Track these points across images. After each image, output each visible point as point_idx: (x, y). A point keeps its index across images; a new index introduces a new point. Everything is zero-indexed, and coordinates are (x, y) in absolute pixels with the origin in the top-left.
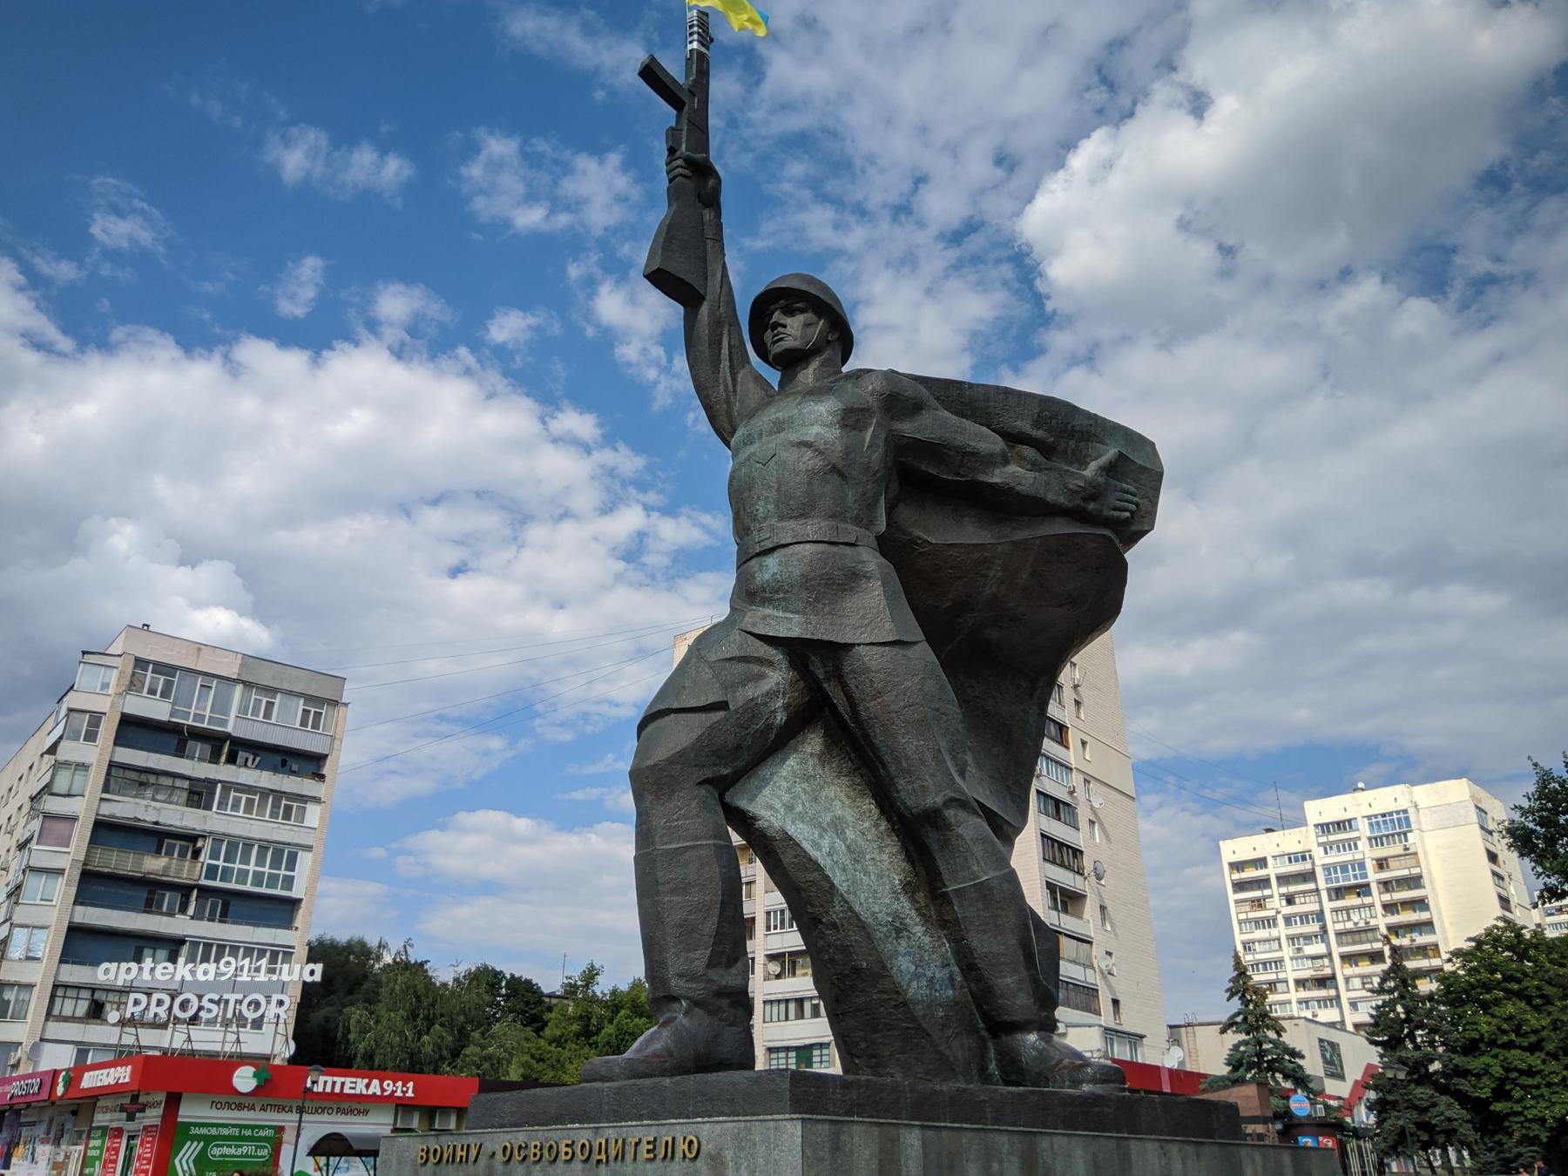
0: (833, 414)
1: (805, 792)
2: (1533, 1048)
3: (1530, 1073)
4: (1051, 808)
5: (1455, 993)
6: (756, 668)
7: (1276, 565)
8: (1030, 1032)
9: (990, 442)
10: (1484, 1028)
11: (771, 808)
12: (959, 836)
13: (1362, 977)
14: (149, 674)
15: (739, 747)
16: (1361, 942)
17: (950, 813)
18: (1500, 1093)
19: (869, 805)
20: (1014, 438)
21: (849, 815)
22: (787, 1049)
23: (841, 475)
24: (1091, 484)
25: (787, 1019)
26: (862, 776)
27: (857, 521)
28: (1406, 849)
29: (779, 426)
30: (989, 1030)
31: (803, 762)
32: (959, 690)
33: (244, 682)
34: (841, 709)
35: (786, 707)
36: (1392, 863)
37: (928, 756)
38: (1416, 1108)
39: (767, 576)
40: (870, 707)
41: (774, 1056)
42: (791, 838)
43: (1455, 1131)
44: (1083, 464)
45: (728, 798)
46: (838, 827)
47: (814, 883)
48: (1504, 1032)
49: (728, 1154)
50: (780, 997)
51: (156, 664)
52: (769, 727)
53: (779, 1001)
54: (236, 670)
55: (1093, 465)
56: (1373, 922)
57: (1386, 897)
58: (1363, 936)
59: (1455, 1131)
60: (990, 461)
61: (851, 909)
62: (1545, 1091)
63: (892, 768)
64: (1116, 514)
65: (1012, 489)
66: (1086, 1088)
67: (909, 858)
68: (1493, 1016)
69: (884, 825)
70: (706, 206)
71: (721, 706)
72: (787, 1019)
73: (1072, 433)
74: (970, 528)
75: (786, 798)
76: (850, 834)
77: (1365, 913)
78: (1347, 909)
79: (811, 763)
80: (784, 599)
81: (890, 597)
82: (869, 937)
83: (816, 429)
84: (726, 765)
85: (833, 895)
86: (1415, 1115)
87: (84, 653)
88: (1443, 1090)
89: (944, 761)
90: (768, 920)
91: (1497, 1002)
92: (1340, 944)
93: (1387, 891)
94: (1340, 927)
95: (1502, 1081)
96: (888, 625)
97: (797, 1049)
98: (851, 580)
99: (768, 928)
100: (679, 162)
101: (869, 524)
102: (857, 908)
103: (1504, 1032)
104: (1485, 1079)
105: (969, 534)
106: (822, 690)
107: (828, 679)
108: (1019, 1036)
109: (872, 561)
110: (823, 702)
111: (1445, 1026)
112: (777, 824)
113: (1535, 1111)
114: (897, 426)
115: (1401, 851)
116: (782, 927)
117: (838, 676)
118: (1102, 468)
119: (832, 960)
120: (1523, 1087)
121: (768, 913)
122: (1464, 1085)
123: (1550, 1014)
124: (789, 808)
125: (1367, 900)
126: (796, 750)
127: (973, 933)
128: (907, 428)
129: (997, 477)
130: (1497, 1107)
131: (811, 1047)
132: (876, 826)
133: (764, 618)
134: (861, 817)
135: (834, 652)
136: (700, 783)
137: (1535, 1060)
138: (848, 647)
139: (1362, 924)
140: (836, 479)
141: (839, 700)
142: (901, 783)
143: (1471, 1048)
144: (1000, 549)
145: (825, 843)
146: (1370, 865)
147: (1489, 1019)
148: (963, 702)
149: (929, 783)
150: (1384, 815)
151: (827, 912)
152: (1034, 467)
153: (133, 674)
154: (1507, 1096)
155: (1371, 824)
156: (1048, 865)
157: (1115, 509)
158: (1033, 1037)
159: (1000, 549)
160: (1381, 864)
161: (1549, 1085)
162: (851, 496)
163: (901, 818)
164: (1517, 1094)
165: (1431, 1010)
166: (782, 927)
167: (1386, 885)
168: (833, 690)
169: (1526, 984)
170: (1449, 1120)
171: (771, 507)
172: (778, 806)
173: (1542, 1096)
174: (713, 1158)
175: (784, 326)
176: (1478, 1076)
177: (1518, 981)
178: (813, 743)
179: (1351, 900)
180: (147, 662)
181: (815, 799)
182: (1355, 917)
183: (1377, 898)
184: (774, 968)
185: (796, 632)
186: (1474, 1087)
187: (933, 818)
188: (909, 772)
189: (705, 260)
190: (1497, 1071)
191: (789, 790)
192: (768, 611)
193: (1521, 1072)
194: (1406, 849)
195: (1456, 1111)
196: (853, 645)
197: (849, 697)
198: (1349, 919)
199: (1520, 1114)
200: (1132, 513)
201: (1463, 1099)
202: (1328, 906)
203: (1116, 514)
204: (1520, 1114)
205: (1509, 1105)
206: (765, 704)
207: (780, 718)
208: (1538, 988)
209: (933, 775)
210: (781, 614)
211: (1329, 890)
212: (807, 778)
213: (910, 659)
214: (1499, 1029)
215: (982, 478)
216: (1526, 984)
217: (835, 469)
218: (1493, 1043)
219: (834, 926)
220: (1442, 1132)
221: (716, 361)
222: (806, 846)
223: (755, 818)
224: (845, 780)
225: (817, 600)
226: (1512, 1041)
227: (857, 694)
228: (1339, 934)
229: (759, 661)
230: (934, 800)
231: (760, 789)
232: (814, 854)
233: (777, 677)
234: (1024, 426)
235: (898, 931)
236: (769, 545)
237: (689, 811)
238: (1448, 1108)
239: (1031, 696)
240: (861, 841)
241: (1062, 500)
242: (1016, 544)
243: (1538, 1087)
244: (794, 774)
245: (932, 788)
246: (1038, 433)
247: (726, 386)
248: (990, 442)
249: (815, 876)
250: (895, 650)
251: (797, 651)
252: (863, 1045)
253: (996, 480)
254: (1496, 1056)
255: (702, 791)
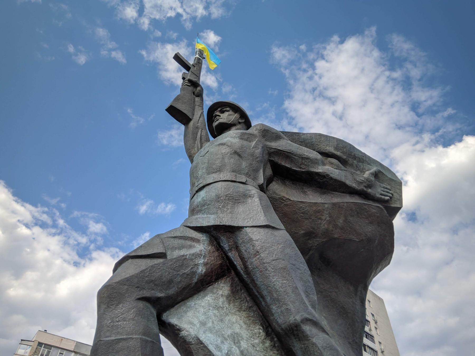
1: (215, 315)
6: (189, 243)
7: (453, 322)
8: (160, 32)
9: (314, 155)
11: (191, 323)
12: (314, 344)
14: (42, 348)
15: (170, 282)
17: (307, 328)
19: (258, 330)
21: (245, 333)
23: (239, 155)
24: (367, 180)
26: (254, 311)
27: (247, 175)
31: (216, 299)
32: (316, 284)
33: (75, 352)
34: (239, 268)
35: (205, 264)
37: (290, 291)
40: (253, 262)
42: (201, 343)
44: (363, 171)
45: (165, 317)
46: (236, 339)
51: (46, 344)
52: (194, 273)
54: (73, 347)
55: (367, 173)
63: (268, 299)
64: (383, 197)
65: (328, 175)
69: (268, 343)
70: (198, 96)
73: (355, 157)
74: (311, 197)
75: (202, 318)
76: (244, 344)
79: (221, 300)
84: (161, 291)
87: (22, 340)
89: (299, 294)
100: (187, 81)
101: (255, 179)
105: (312, 198)
106: (228, 258)
107: (230, 250)
110: (229, 267)
114: (268, 144)
118: (372, 174)
124: (203, 324)
126: (212, 292)
128: (274, 145)
129: (320, 169)
134: (253, 336)
135: (232, 230)
136: (140, 299)
138: (240, 228)
140: (237, 157)
141: (238, 263)
142: (274, 308)
144: (326, 206)
148: (319, 292)
149: (291, 306)
153: (37, 348)
157: (382, 195)
159: (326, 206)
162: (244, 164)
163: (278, 335)
168: (233, 255)
172: (196, 322)
175: (220, 116)
178: (222, 289)
180: (42, 344)
181: (222, 320)
187: (295, 331)
188: (278, 300)
189: (194, 110)
191: (205, 313)
196: (242, 227)
197: (242, 258)
200: (391, 198)
203: (383, 197)
206: (192, 260)
207: (201, 270)
209: (293, 302)
210: (205, 216)
212: (217, 308)
213: (275, 236)
217: (236, 153)
221: (195, 139)
222: (212, 348)
223: (180, 330)
224: (244, 314)
229: (192, 239)
231: (186, 312)
233: (201, 247)
236: (202, 185)
237: (131, 318)
239: (356, 295)
240: (251, 350)
241: (354, 185)
242: (334, 204)
244: (209, 305)
245: (293, 310)
246: (338, 153)
248: (314, 155)
250: (267, 230)
255: (141, 304)
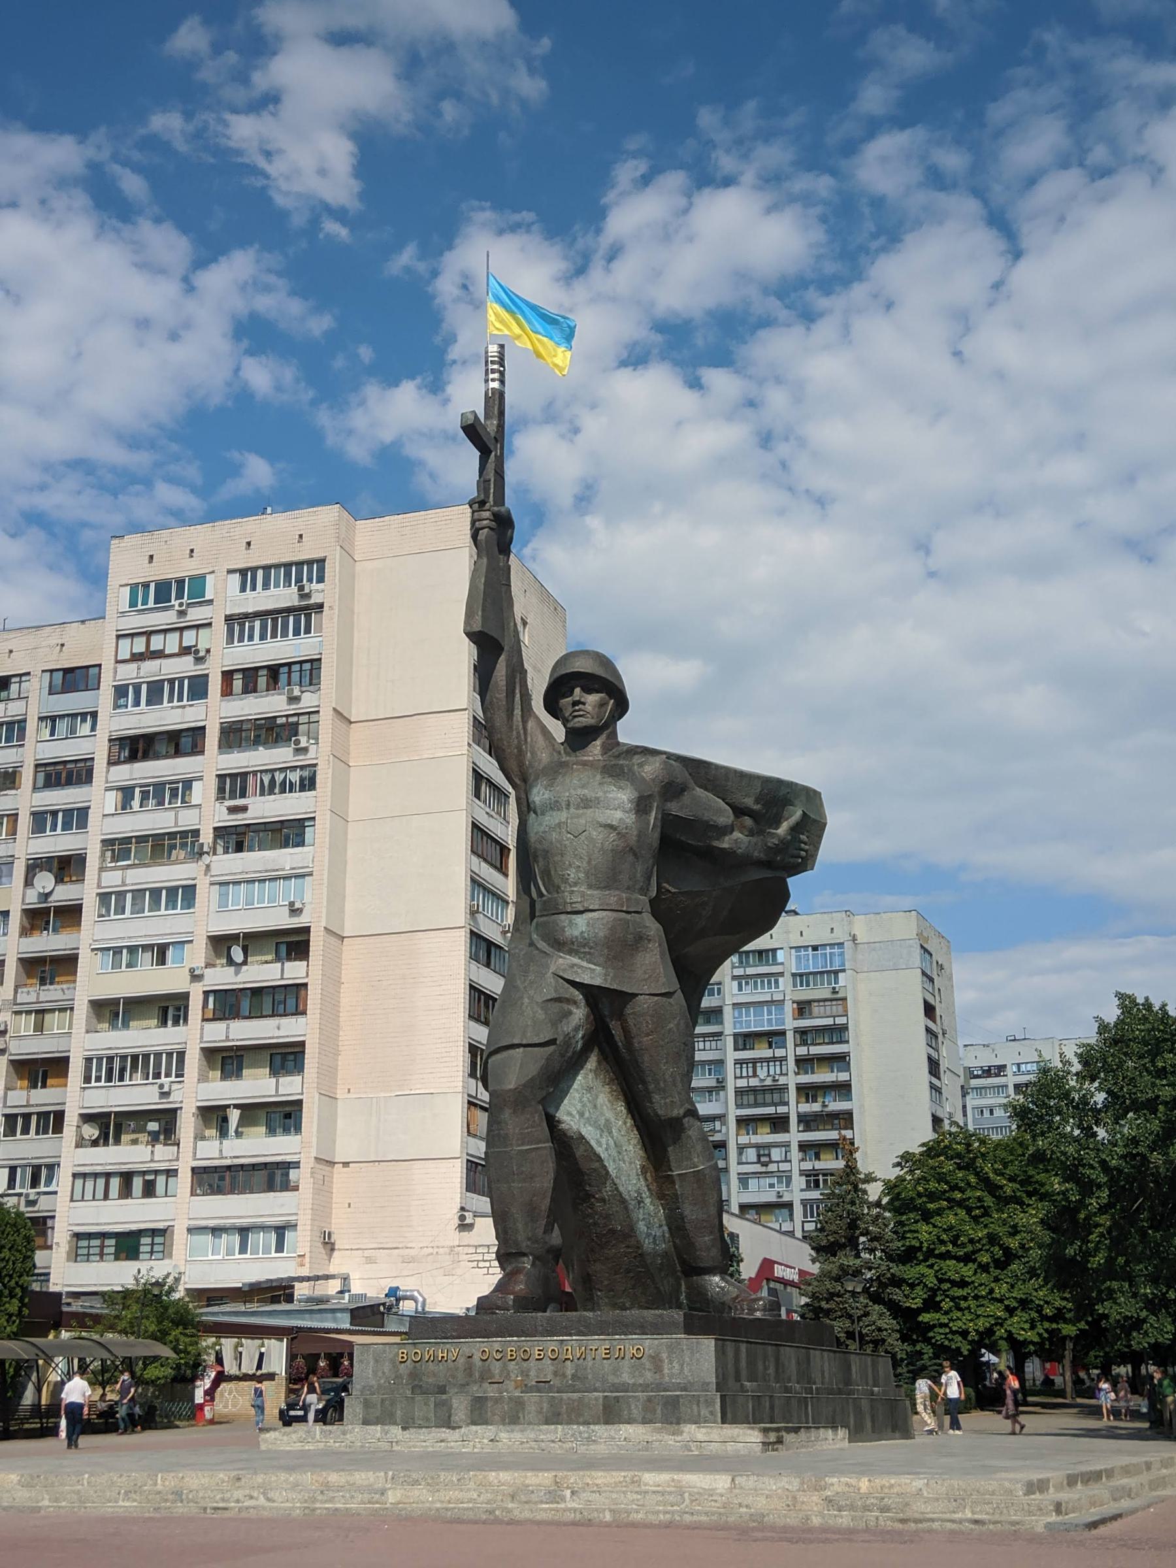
0: (630, 801)
2: (967, 1259)
3: (963, 1284)
4: (482, 954)
5: (900, 1200)
8: (715, 1275)
10: (924, 1236)
13: (758, 1147)
16: (765, 1105)
18: (931, 1304)
19: (621, 1107)
20: (739, 811)
22: (103, 1235)
23: (635, 855)
25: (106, 1197)
28: (834, 991)
29: (586, 803)
30: (683, 1272)
34: (617, 1038)
36: (816, 1010)
38: (850, 1317)
39: (576, 933)
41: (84, 1243)
42: (583, 1138)
43: (884, 1341)
46: (607, 1128)
47: (595, 1170)
48: (942, 1242)
49: (664, 1356)
50: (99, 1169)
53: (96, 1175)
56: (782, 1080)
57: (802, 1051)
58: (768, 1097)
59: (884, 1341)
60: (727, 830)
61: (617, 1189)
62: (972, 1303)
63: (652, 1087)
64: (792, 860)
66: (758, 1314)
67: (645, 1147)
68: (935, 1226)
69: (630, 1122)
71: (552, 1042)
72: (106, 1197)
77: (775, 1069)
78: (754, 1062)
80: (589, 953)
81: (662, 954)
82: (626, 1208)
83: (619, 814)
85: (606, 1180)
86: (848, 1323)
88: (876, 1298)
90: (88, 1069)
91: (939, 1212)
92: (739, 1106)
93: (804, 1043)
94: (742, 1083)
95: (934, 1291)
96: (663, 980)
97: (117, 1235)
98: (639, 941)
99: (87, 1079)
102: (621, 1189)
103: (942, 1242)
104: (918, 1290)
108: (707, 1277)
109: (653, 927)
111: (889, 1235)
112: (575, 1127)
113: (960, 1323)
115: (827, 994)
116: (109, 1078)
117: (620, 1016)
119: (595, 1224)
120: (953, 1299)
121: (89, 1060)
122: (896, 1294)
123: (986, 1226)
124: (581, 1114)
125: (780, 1053)
127: (686, 1205)
128: (674, 808)
129: (725, 843)
130: (925, 1317)
131: (140, 1233)
132: (625, 1123)
133: (573, 966)
135: (621, 999)
137: (967, 1271)
139: (769, 1082)
140: (631, 858)
142: (656, 1097)
143: (908, 1256)
145: (604, 1141)
146: (789, 1008)
147: (930, 1228)
150: (815, 948)
151: (600, 1191)
152: (751, 833)
154: (937, 1307)
155: (798, 958)
156: (472, 1024)
158: (717, 1279)
160: (803, 1008)
161: (976, 1297)
164: (945, 1305)
165: (878, 1216)
166: (109, 1078)
167: (803, 1035)
169: (969, 1193)
170: (880, 1330)
171: (582, 875)
172: (575, 1113)
173: (969, 1308)
174: (653, 1357)
175: (584, 704)
176: (912, 1286)
177: (962, 1191)
179: (762, 1051)
182: (762, 1072)
183: (791, 1050)
184: (91, 1132)
185: (598, 982)
186: (907, 1296)
190: (931, 1281)
192: (576, 960)
193: (954, 1283)
194: (834, 991)
195: (888, 1322)
196: (637, 995)
198: (755, 1075)
199: (946, 1325)
201: (896, 1309)
202: (731, 1055)
204: (946, 1325)
205: (937, 1316)
208: (980, 1199)
209: (679, 1093)
210: (585, 964)
211: (735, 1035)
212: (589, 1089)
214: (938, 1237)
215: (716, 844)
216: (969, 1193)
218: (930, 1253)
219: (603, 1200)
220: (871, 1341)
222: (593, 1143)
225: (615, 958)
226: (948, 1251)
227: (634, 1030)
228: (739, 1092)
230: (678, 1112)
232: (598, 1150)
233: (580, 1013)
234: (749, 802)
235: (639, 1203)
236: (580, 907)
238: (882, 1320)
243: (965, 1298)
247: (518, 733)
249: (597, 1165)
251: (592, 994)
252: (606, 1283)
253: (725, 845)
254: (931, 1266)
